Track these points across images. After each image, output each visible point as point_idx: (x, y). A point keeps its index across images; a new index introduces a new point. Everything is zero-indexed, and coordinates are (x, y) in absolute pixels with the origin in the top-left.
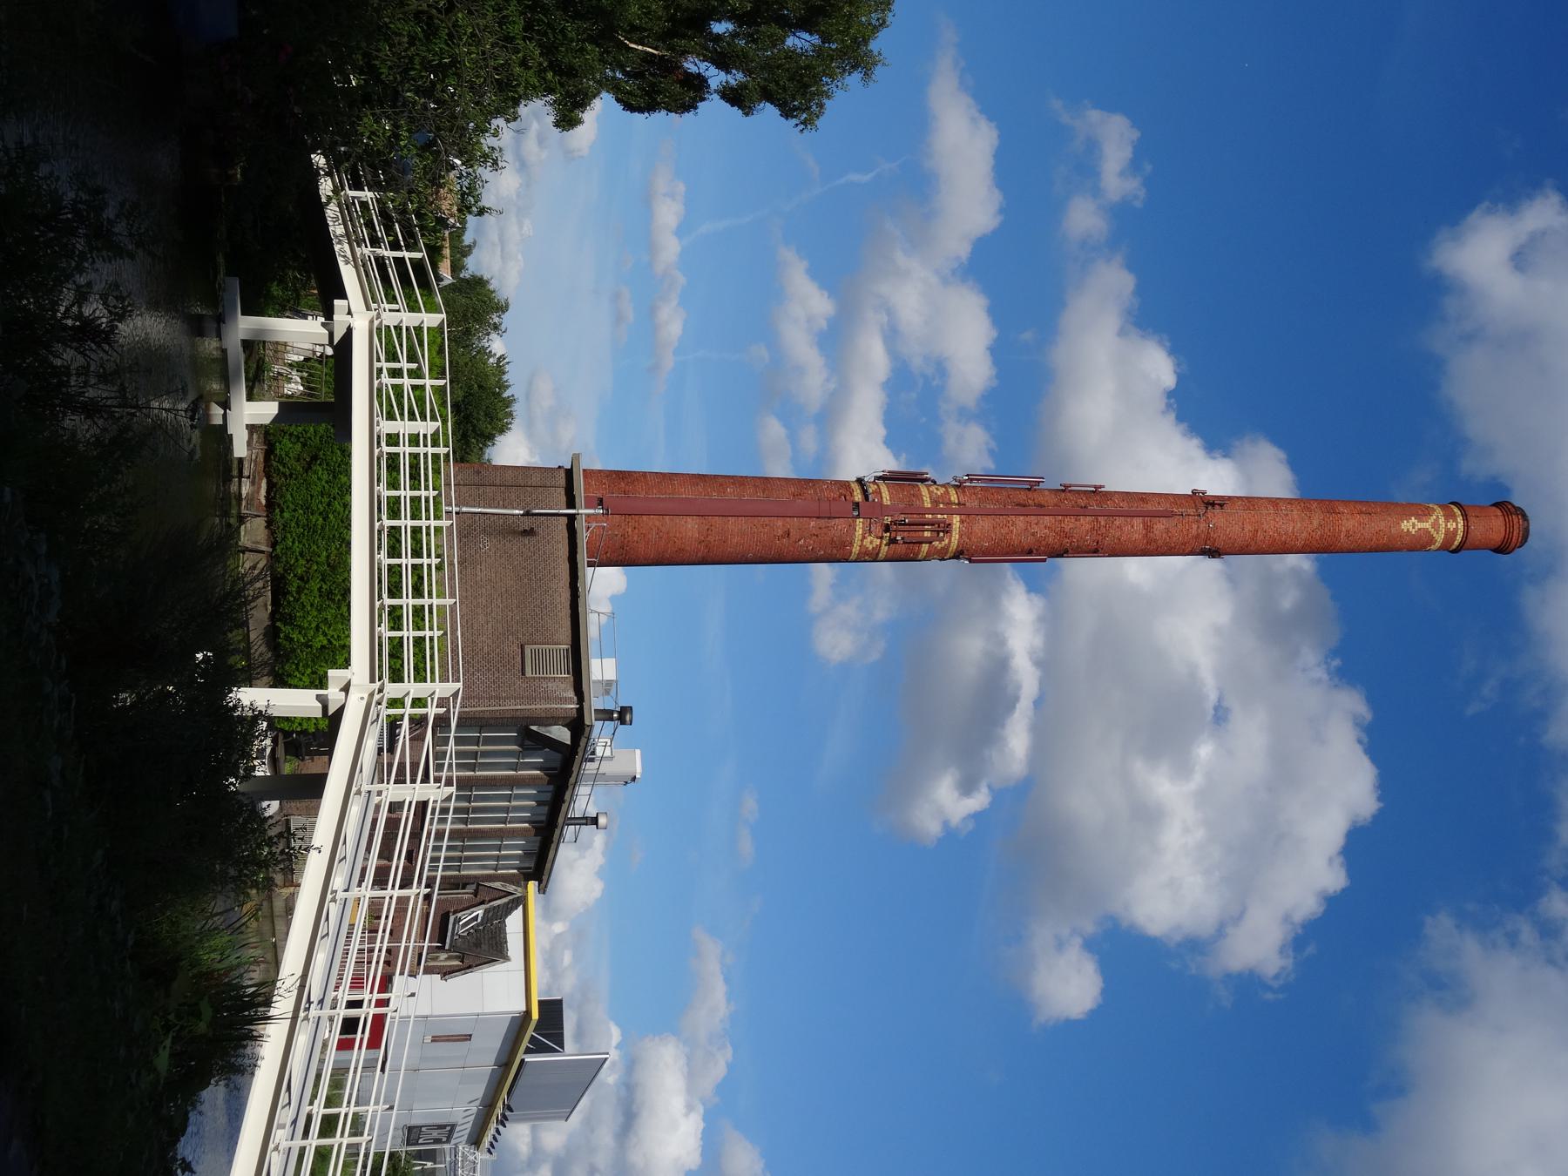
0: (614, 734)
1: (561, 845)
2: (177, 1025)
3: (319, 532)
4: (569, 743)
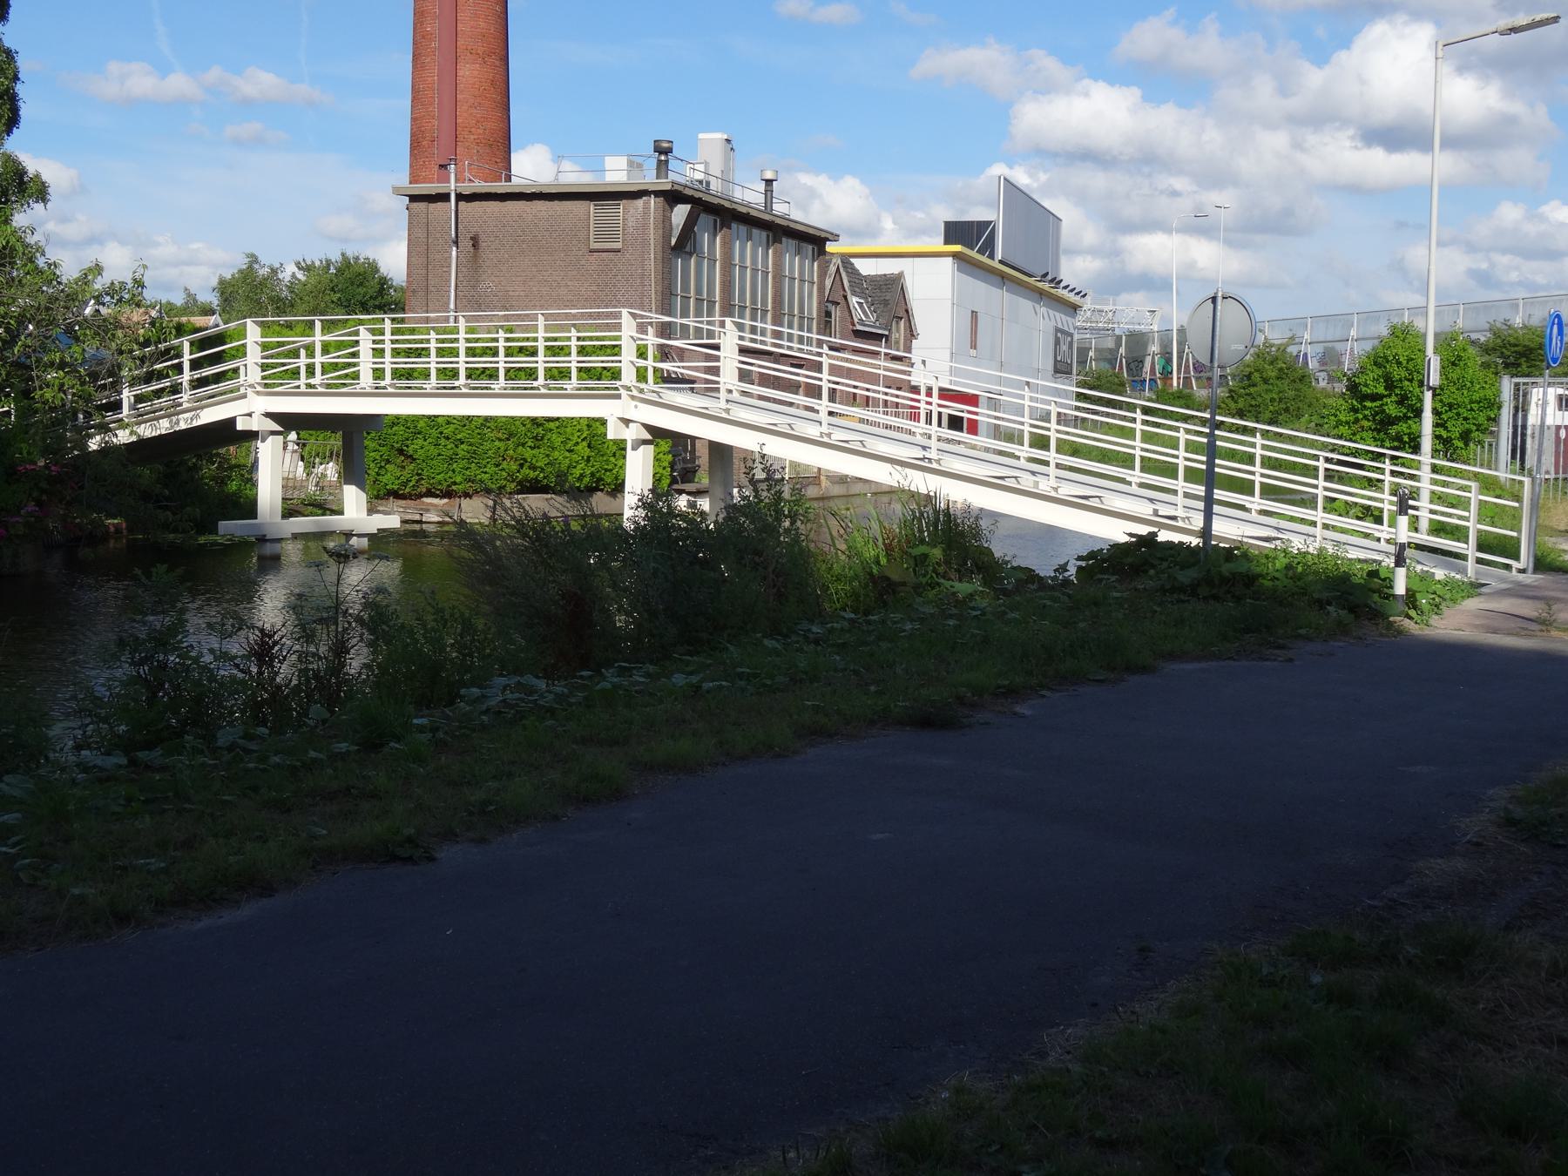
0: (682, 160)
1: (791, 217)
2: (932, 576)
3: (474, 448)
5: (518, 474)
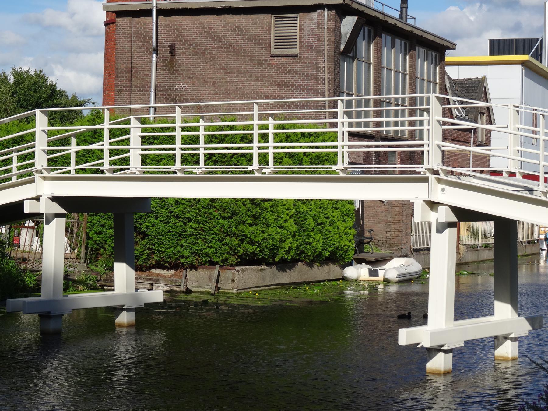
3: (201, 225)
4: (355, 18)
5: (239, 249)
